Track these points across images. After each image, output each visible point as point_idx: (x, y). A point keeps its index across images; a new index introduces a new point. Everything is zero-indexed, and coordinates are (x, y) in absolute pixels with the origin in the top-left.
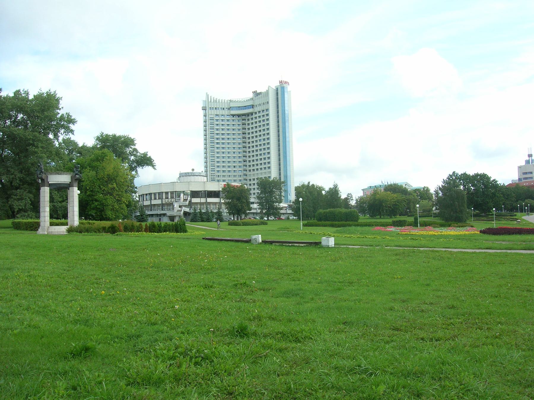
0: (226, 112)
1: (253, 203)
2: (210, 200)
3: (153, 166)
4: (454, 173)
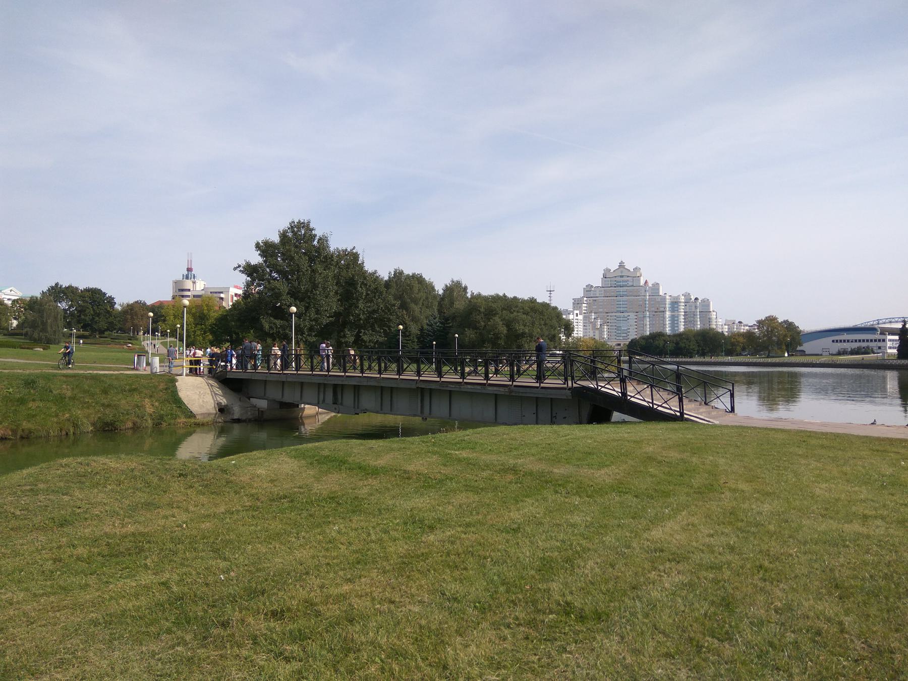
4: (57, 284)
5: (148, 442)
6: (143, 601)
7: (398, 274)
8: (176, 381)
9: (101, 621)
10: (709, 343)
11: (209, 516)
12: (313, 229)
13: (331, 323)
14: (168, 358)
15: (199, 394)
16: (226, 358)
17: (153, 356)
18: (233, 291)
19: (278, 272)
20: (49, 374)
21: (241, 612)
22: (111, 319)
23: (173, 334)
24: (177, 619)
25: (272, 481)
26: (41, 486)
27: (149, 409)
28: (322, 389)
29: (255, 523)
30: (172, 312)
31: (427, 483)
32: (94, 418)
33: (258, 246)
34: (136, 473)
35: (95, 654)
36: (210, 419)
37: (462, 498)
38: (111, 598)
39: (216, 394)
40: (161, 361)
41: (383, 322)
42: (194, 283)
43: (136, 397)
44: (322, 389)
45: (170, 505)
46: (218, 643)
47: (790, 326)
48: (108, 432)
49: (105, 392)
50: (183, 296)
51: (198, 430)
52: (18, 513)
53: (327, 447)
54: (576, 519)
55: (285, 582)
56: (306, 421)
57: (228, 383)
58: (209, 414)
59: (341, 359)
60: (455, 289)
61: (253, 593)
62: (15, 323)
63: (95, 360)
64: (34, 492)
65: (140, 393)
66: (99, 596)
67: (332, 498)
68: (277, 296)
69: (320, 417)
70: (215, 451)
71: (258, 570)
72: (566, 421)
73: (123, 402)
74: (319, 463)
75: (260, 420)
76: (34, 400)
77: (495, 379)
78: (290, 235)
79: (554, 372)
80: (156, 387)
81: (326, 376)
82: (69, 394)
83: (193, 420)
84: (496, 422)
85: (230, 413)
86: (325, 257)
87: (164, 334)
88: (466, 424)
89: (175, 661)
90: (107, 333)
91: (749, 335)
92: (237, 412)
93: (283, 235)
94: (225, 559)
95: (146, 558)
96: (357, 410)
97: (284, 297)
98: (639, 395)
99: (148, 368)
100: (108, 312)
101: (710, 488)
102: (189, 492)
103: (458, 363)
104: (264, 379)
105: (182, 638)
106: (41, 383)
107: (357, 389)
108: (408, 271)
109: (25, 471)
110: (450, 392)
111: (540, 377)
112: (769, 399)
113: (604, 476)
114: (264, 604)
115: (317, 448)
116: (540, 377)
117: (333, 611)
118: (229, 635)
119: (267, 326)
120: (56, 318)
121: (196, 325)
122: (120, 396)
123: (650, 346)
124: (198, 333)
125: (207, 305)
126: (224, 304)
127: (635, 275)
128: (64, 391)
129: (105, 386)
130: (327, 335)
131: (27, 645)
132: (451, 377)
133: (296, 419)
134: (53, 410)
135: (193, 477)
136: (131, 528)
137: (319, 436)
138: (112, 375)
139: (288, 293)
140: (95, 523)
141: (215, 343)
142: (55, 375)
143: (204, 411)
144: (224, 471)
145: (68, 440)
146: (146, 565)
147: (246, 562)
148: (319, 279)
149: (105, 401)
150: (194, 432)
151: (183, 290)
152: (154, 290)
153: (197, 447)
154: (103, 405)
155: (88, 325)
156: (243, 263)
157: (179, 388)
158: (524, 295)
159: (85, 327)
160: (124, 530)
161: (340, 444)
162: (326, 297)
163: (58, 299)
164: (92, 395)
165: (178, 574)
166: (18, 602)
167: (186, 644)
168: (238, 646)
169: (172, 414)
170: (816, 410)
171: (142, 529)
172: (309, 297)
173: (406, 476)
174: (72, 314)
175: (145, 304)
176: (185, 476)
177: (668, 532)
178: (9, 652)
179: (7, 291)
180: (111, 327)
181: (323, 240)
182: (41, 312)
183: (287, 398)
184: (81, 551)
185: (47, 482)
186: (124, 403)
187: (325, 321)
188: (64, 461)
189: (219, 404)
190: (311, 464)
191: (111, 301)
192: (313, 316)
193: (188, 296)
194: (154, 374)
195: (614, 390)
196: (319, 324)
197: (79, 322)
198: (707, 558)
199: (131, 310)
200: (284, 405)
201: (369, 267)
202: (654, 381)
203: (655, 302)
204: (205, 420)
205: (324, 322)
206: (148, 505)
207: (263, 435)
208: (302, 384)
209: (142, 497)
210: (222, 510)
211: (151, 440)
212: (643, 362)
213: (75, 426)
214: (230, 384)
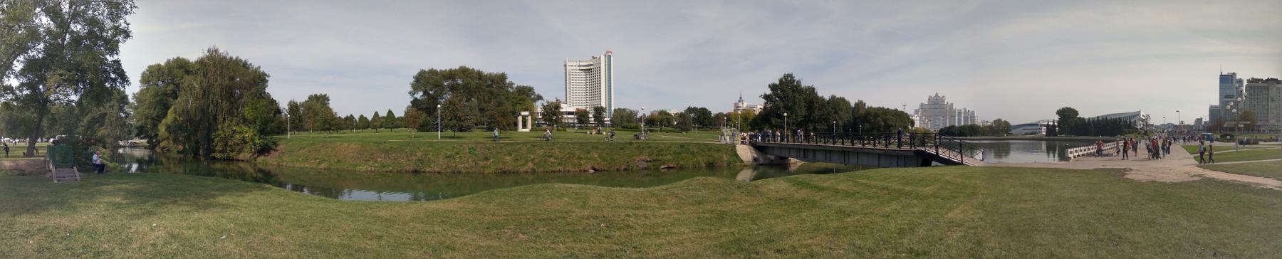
7: (833, 97)
10: (973, 130)
14: (733, 136)
16: (756, 136)
17: (727, 136)
31: (847, 195)
37: (863, 201)
41: (826, 120)
47: (1006, 123)
48: (711, 167)
53: (801, 177)
54: (915, 210)
59: (807, 137)
60: (860, 104)
61: (769, 241)
67: (803, 201)
72: (910, 165)
75: (771, 165)
77: (878, 147)
79: (906, 143)
84: (879, 167)
88: (865, 168)
91: (991, 127)
93: (781, 80)
96: (815, 160)
98: (944, 153)
101: (973, 194)
103: (861, 139)
107: (814, 151)
108: (838, 96)
110: (858, 153)
111: (899, 146)
112: (998, 155)
113: (928, 190)
116: (899, 146)
117: (804, 251)
123: (949, 132)
127: (943, 99)
129: (709, 148)
130: (802, 127)
132: (858, 145)
137: (797, 172)
145: (696, 170)
152: (727, 108)
153: (745, 175)
158: (892, 108)
161: (807, 176)
170: (1017, 158)
173: (837, 191)
177: (956, 214)
181: (799, 82)
186: (717, 155)
195: (933, 151)
198: (972, 224)
201: (820, 94)
202: (950, 147)
203: (950, 111)
206: (726, 199)
207: (772, 171)
209: (723, 196)
212: (945, 139)
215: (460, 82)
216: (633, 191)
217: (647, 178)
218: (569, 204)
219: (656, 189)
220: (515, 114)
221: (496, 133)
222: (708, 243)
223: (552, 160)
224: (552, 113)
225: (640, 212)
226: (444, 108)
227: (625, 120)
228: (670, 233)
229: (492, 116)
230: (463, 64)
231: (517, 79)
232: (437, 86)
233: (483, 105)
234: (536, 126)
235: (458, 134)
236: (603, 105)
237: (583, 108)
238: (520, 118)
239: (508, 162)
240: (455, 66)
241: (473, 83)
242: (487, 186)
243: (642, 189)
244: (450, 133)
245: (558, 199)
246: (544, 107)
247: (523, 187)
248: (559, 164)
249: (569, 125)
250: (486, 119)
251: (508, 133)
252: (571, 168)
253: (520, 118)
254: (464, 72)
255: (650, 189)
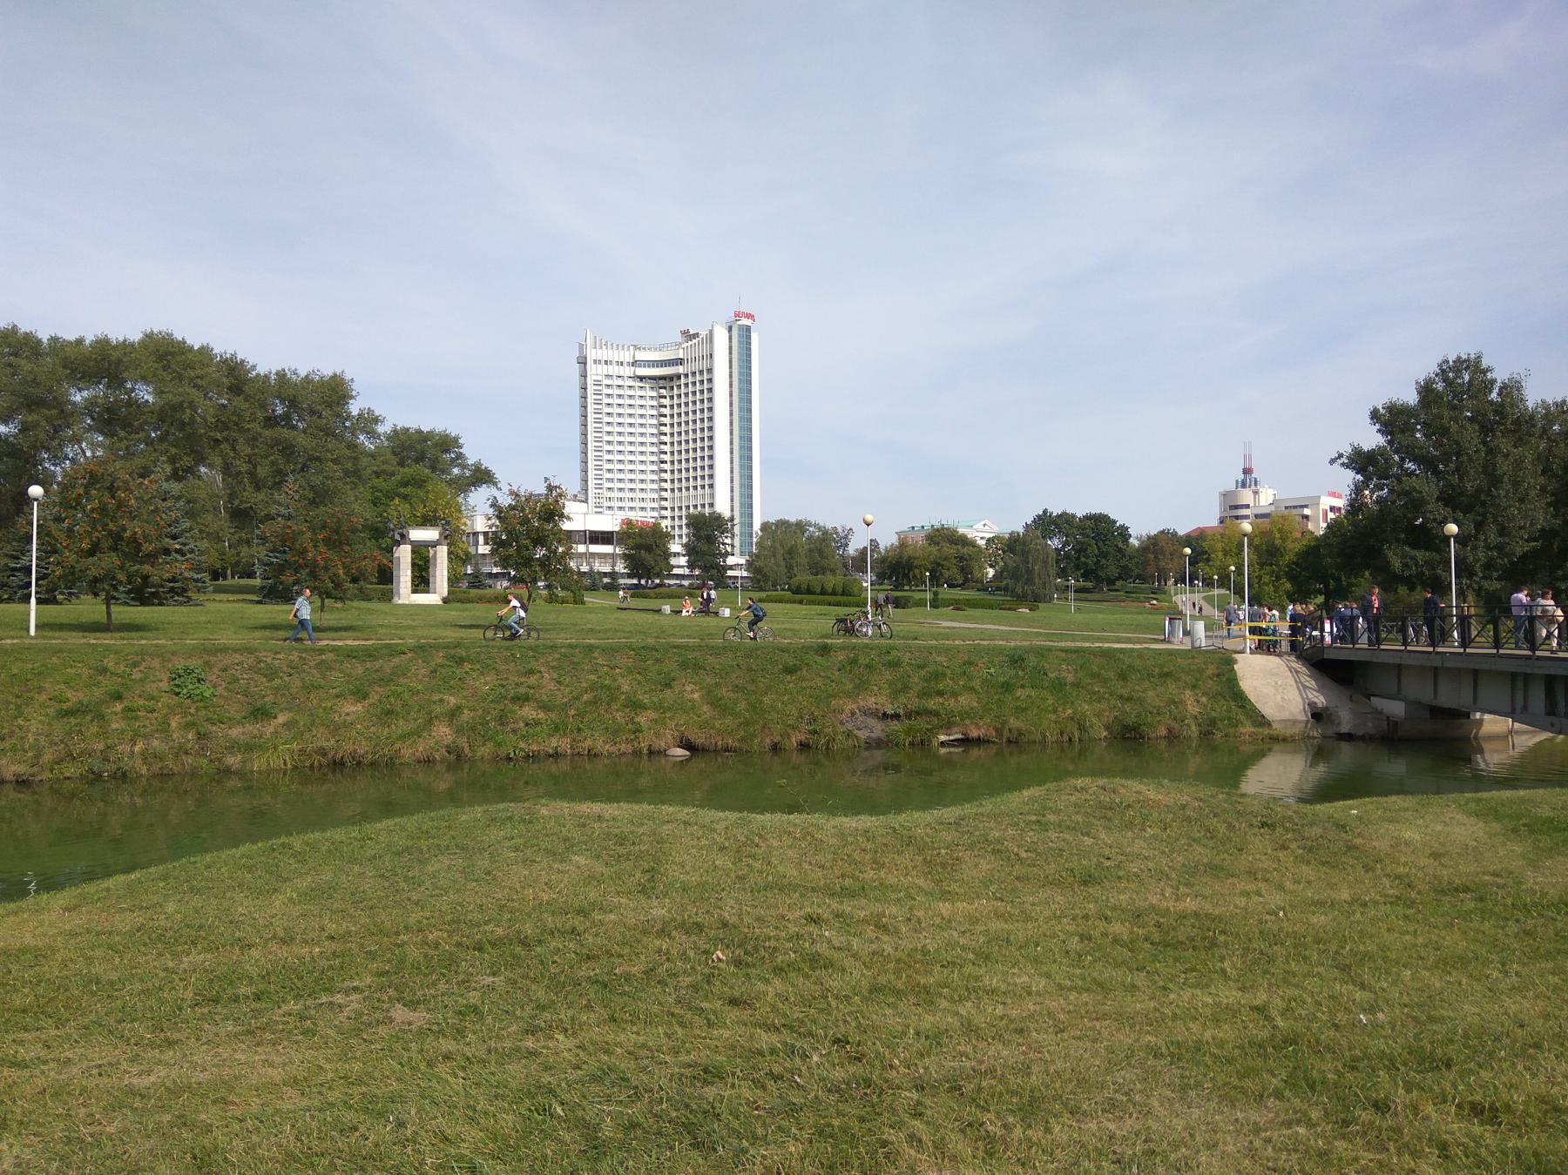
0: (629, 371)
1: (676, 555)
2: (594, 548)
3: (495, 484)
4: (1045, 511)
5: (1194, 762)
6: (1227, 1032)
8: (1235, 662)
9: (1164, 1050)
11: (1322, 904)
12: (1488, 370)
13: (1534, 553)
15: (1275, 686)
17: (1195, 620)
18: (1326, 502)
19: (1415, 460)
20: (1042, 648)
21: (1408, 1091)
22: (1124, 562)
23: (1224, 582)
24: (1290, 1076)
25: (1436, 855)
26: (1051, 817)
27: (1193, 709)
28: (1520, 685)
29: (1411, 929)
30: (1219, 545)
32: (1109, 717)
33: (1375, 416)
34: (1189, 812)
35: (1162, 1105)
36: (1297, 730)
38: (1175, 1017)
39: (1305, 687)
40: (1207, 628)
42: (1256, 493)
43: (1172, 687)
44: (1520, 685)
45: (1252, 874)
46: (1372, 1135)
48: (1130, 739)
49: (1123, 676)
50: (1237, 518)
51: (1276, 747)
52: (1024, 855)
55: (1491, 1054)
56: (1486, 746)
57: (1323, 666)
58: (1295, 722)
62: (991, 572)
63: (1074, 624)
64: (1042, 826)
65: (1177, 680)
66: (1156, 1009)
68: (1417, 505)
69: (1518, 740)
70: (1307, 787)
71: (1432, 1019)
73: (1151, 693)
74: (1532, 832)
75: (1391, 738)
76: (1023, 686)
78: (1440, 386)
80: (1201, 671)
81: (1528, 658)
82: (1070, 678)
83: (1266, 731)
85: (1332, 722)
86: (1517, 422)
87: (1208, 583)
89: (1296, 1151)
90: (1119, 584)
92: (1346, 720)
93: (1426, 390)
94: (1363, 987)
95: (1222, 959)
97: (1430, 507)
99: (1187, 640)
100: (1120, 550)
102: (1281, 855)
104: (1397, 661)
105: (1305, 1114)
106: (1032, 660)
109: (1025, 793)
114: (1454, 1086)
115: (1523, 801)
118: (1390, 1129)
119: (1396, 563)
120: (1045, 562)
121: (1262, 565)
122: (1146, 684)
124: (1266, 579)
125: (1280, 531)
126: (1310, 526)
128: (1064, 674)
129: (1122, 667)
131: (1060, 1065)
133: (1466, 739)
134: (1050, 702)
135: (1286, 830)
136: (1190, 904)
137: (1509, 780)
138: (1132, 650)
139: (1438, 499)
140: (1133, 886)
141: (1299, 596)
142: (1050, 649)
143: (1286, 715)
144: (1342, 827)
145: (1072, 751)
146: (1223, 971)
147: (1406, 999)
148: (1503, 467)
149: (1123, 692)
150: (1270, 750)
151: (1237, 507)
152: (1193, 513)
153: (1277, 776)
154: (1121, 697)
155: (1093, 571)
156: (1347, 450)
157: (1239, 674)
159: (1086, 576)
160: (1180, 906)
162: (1521, 500)
163: (1047, 534)
164: (1105, 681)
165: (1283, 998)
166: (1039, 994)
167: (1311, 1125)
168: (1411, 1154)
169: (1229, 718)
171: (1208, 908)
172: (1483, 503)
174: (1067, 556)
175: (1175, 534)
176: (1272, 827)
178: (1035, 1069)
179: (979, 526)
180: (1125, 574)
181: (1511, 390)
182: (1025, 554)
183: (1446, 699)
184: (1117, 928)
185: (1058, 812)
186: (1153, 696)
187: (1520, 548)
188: (1079, 782)
189: (1312, 705)
190: (1515, 830)
191: (1124, 533)
192: (1493, 538)
193: (1246, 517)
194: (1196, 650)
196: (1507, 555)
197: (1077, 567)
199: (1155, 545)
200: (1437, 712)
204: (1289, 732)
205: (1519, 551)
206: (1214, 869)
207: (1397, 767)
208: (1476, 674)
209: (1202, 853)
210: (1345, 895)
211: (1198, 760)
213: (1082, 728)
214: (1328, 668)
215: (146, 394)
216: (830, 825)
217: (886, 782)
218: (592, 879)
219: (919, 821)
220: (385, 536)
221: (304, 608)
222: (1125, 1038)
223: (529, 712)
224: (531, 534)
225: (859, 909)
226: (66, 500)
227: (801, 563)
228: (973, 991)
229: (287, 541)
230: (159, 326)
231: (392, 401)
232: (33, 404)
233: (251, 497)
234: (467, 585)
235: (122, 613)
236: (723, 507)
237: (646, 517)
238: (404, 554)
239: (354, 723)
240: (126, 327)
241: (207, 406)
242: (259, 824)
243: (866, 821)
244: (89, 608)
245: (548, 861)
246: (501, 513)
247: (410, 822)
248: (556, 729)
249: (594, 583)
250: (259, 552)
251: (354, 611)
252: (601, 744)
253: (404, 554)
254: (165, 355)
255: (900, 820)
